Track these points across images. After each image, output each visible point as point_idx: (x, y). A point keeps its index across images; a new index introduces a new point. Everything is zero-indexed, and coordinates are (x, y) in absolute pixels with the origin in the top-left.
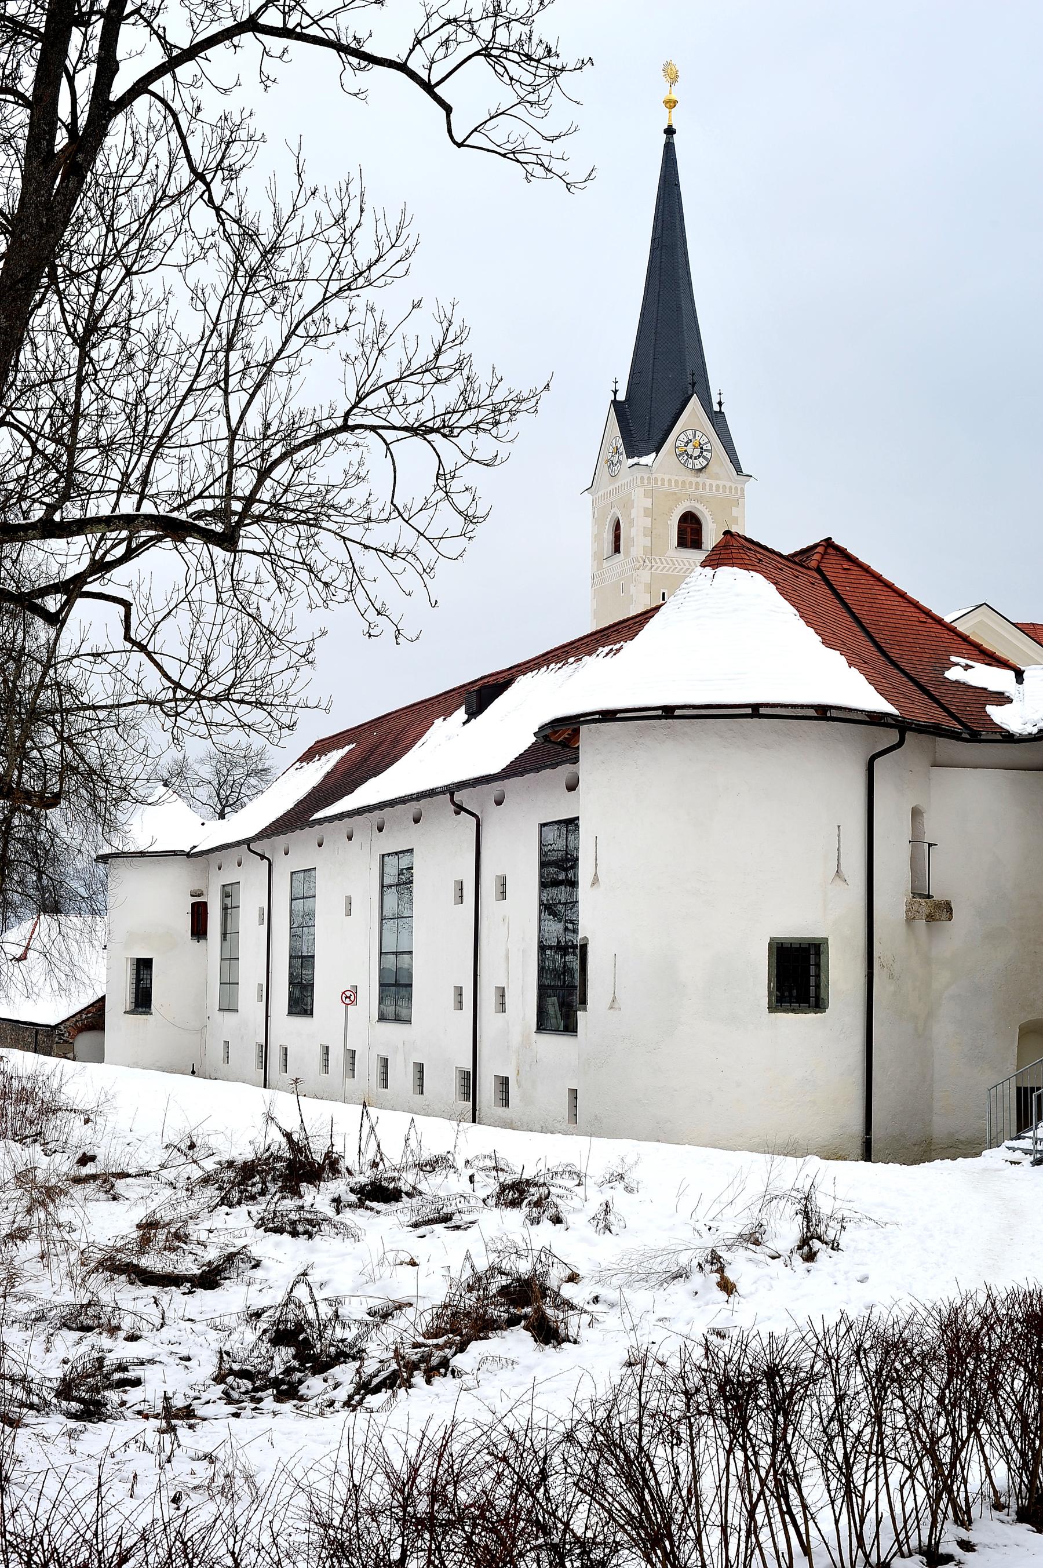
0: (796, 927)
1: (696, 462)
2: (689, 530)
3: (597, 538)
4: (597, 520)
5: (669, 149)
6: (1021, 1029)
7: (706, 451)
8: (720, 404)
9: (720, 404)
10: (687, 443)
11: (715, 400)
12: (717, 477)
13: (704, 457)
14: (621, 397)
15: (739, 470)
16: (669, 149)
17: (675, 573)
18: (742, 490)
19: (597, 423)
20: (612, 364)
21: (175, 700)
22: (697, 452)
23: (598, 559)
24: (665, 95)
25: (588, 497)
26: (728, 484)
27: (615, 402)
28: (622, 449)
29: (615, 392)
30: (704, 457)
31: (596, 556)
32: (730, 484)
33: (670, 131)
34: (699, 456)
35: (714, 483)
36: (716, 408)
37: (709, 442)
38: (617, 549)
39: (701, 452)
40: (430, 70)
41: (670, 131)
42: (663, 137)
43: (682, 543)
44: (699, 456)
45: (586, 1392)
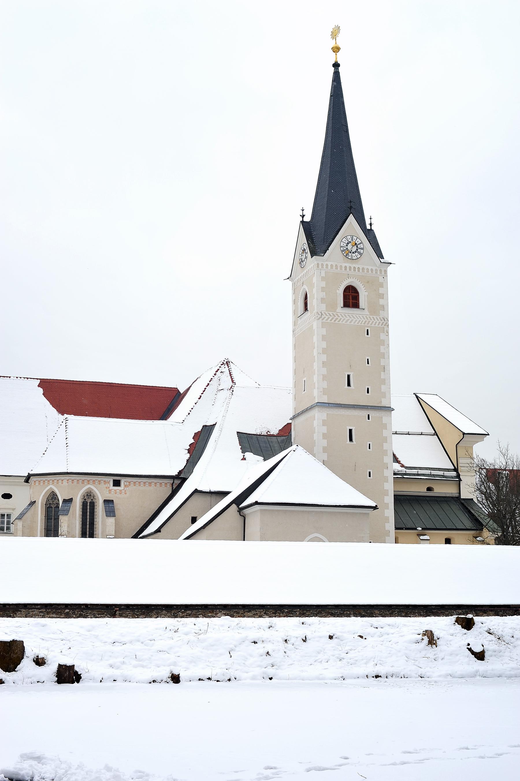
0: (112, 483)
1: (350, 252)
2: (351, 296)
3: (295, 302)
4: (295, 291)
7: (360, 248)
8: (371, 224)
9: (371, 224)
10: (348, 243)
11: (368, 222)
14: (307, 219)
15: (380, 255)
17: (344, 322)
18: (386, 272)
19: (292, 236)
23: (298, 317)
24: (332, 44)
25: (289, 283)
27: (302, 222)
28: (308, 250)
29: (303, 216)
31: (295, 312)
33: (336, 65)
36: (368, 227)
38: (306, 309)
40: (437, 435)
41: (336, 65)
42: (332, 69)
43: (346, 305)
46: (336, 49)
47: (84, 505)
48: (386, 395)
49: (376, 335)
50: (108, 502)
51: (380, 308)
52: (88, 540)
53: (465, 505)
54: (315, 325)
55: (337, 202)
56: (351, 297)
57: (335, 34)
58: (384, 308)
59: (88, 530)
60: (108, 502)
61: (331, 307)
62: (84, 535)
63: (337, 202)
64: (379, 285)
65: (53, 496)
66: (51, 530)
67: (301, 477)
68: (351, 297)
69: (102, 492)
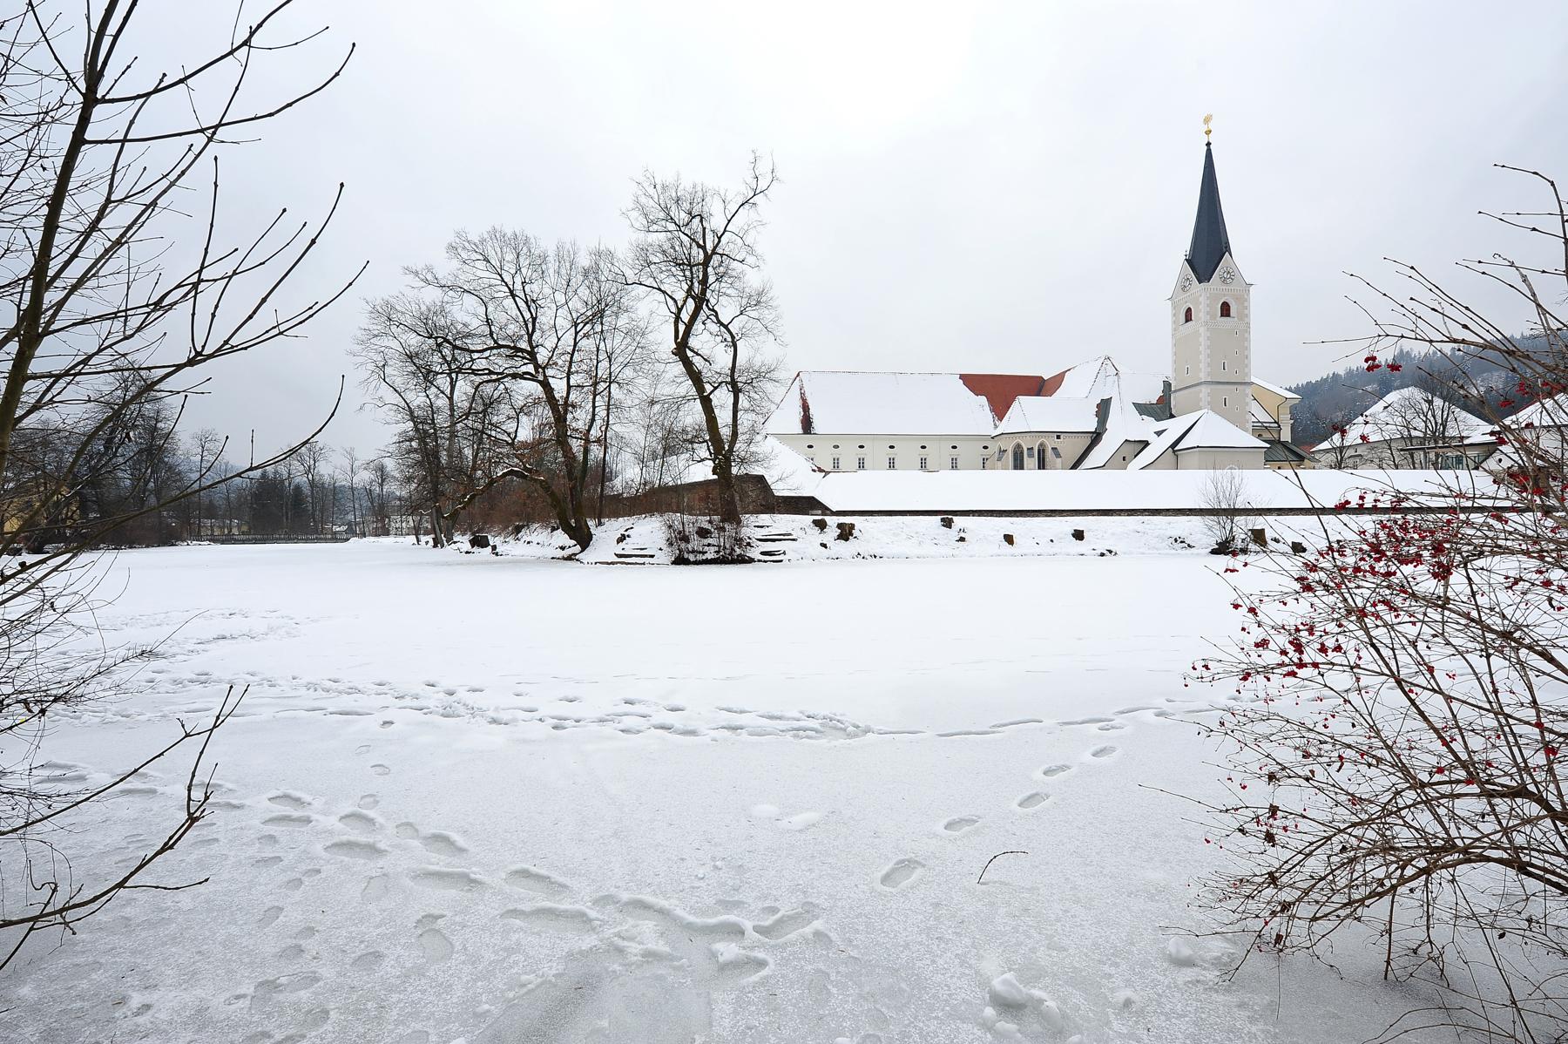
27: (583, 550)
33: (1208, 144)
41: (1208, 144)
46: (1208, 132)
47: (1015, 454)
48: (1248, 374)
49: (1242, 337)
50: (1054, 449)
51: (1244, 316)
52: (892, 472)
53: (1284, 444)
54: (1202, 330)
55: (1209, 249)
56: (1225, 310)
57: (1207, 120)
58: (1247, 316)
59: (1042, 465)
60: (1054, 449)
61: (1213, 317)
62: (1016, 468)
63: (1209, 249)
64: (1243, 300)
65: (1019, 446)
66: (1019, 464)
67: (1213, 429)
68: (1225, 310)
69: (1050, 443)
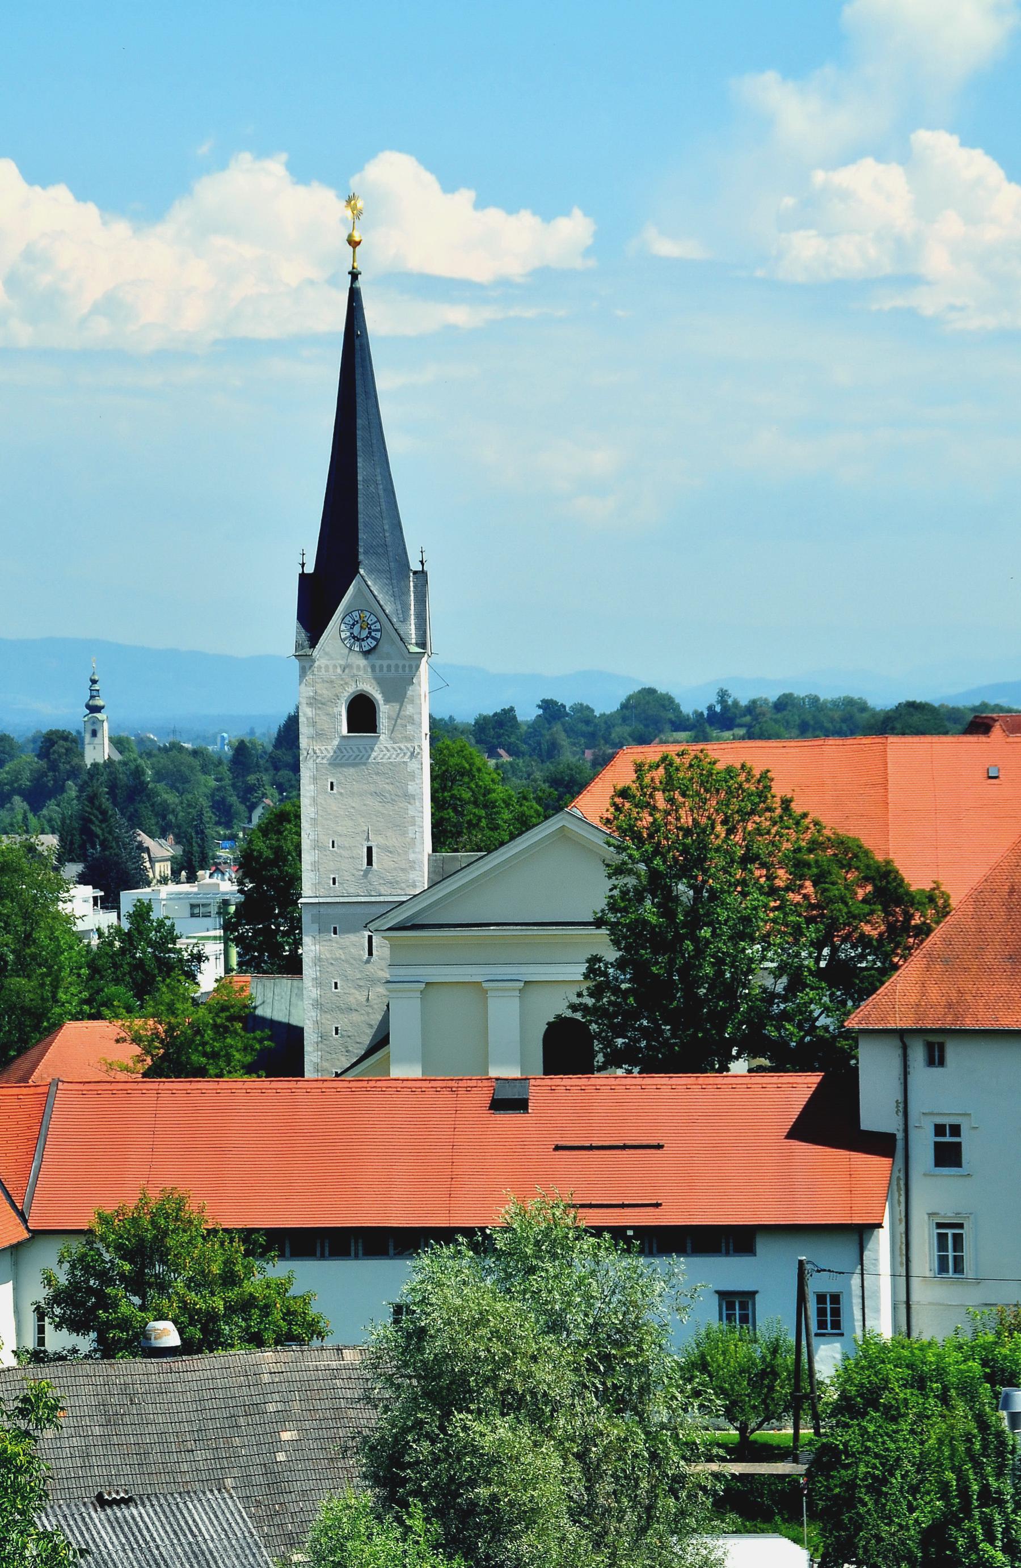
5: (354, 297)
6: (388, 1043)
10: (354, 625)
12: (388, 657)
13: (373, 638)
14: (310, 569)
16: (354, 297)
20: (303, 547)
21: (564, 1349)
22: (365, 633)
26: (401, 663)
27: (303, 577)
29: (303, 565)
30: (373, 638)
32: (404, 662)
33: (354, 276)
34: (367, 637)
35: (385, 663)
37: (378, 621)
39: (370, 633)
41: (354, 276)
44: (367, 637)
45: (600, 784)
